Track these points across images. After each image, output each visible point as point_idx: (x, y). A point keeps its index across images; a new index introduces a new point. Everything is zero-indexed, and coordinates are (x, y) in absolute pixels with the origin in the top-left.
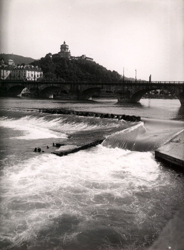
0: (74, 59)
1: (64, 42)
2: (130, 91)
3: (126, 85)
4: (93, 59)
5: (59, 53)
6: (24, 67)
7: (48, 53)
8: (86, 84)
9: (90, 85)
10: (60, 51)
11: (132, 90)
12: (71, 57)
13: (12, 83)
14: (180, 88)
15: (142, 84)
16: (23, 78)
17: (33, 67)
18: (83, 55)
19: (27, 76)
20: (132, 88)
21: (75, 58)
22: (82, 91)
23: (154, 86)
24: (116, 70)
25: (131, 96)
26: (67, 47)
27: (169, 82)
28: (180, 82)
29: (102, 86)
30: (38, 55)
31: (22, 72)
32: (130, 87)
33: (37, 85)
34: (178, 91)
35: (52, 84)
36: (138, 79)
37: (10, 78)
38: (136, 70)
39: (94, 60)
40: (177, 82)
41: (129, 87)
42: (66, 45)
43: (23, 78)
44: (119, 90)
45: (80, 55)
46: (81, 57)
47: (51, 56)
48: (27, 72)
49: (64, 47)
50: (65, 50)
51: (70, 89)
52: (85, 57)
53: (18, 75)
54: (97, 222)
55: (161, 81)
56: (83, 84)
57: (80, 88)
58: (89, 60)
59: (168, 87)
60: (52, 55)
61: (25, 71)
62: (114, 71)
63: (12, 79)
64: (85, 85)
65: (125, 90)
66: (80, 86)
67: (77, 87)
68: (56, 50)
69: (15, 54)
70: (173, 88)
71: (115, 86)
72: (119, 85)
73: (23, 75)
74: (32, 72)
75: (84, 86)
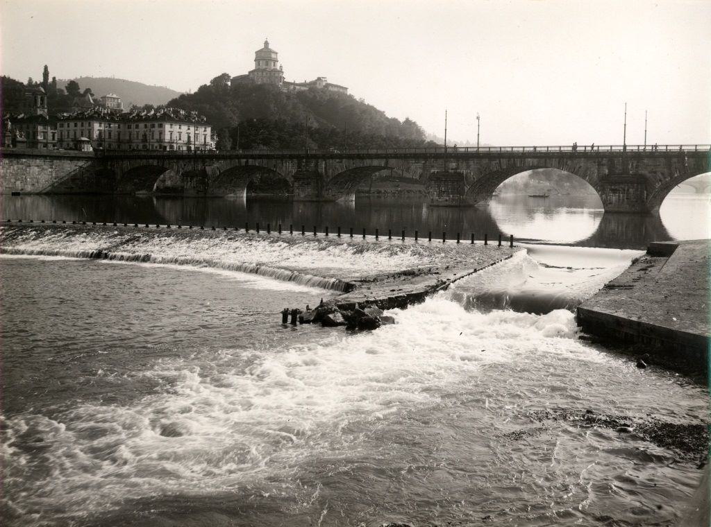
0: (295, 88)
1: (266, 43)
2: (463, 174)
3: (452, 159)
4: (346, 89)
5: (250, 72)
6: (158, 114)
7: (219, 74)
8: (340, 157)
9: (353, 160)
10: (252, 67)
11: (470, 171)
12: (285, 83)
13: (129, 158)
14: (600, 164)
15: (544, 153)
16: (156, 144)
17: (182, 112)
18: (319, 79)
19: (167, 137)
20: (468, 167)
21: (298, 87)
22: (331, 178)
23: (529, 159)
24: (412, 119)
25: (466, 188)
26: (273, 56)
27: (558, 149)
28: (549, 149)
29: (387, 163)
30: (189, 82)
31: (68, 126)
32: (465, 164)
33: (204, 163)
34: (596, 171)
35: (245, 160)
36: (450, 144)
37: (119, 146)
38: (478, 118)
39: (349, 92)
40: (632, 146)
41: (462, 163)
42: (271, 52)
43: (156, 144)
44: (434, 173)
45: (311, 78)
46: (314, 83)
47: (229, 83)
48: (167, 127)
49: (265, 56)
50: (267, 64)
51: (296, 173)
52: (324, 84)
53: (141, 137)
54: (470, 489)
55: (599, 145)
56: (333, 157)
57: (325, 168)
58: (336, 89)
59: (569, 162)
60: (231, 78)
61: (90, 123)
62: (407, 119)
63: (125, 147)
64: (338, 160)
65: (450, 171)
66: (324, 162)
67: (316, 165)
68: (240, 65)
69: (104, 76)
70: (582, 164)
71: (423, 162)
72: (434, 158)
73: (157, 136)
74: (171, 127)
75: (335, 163)
